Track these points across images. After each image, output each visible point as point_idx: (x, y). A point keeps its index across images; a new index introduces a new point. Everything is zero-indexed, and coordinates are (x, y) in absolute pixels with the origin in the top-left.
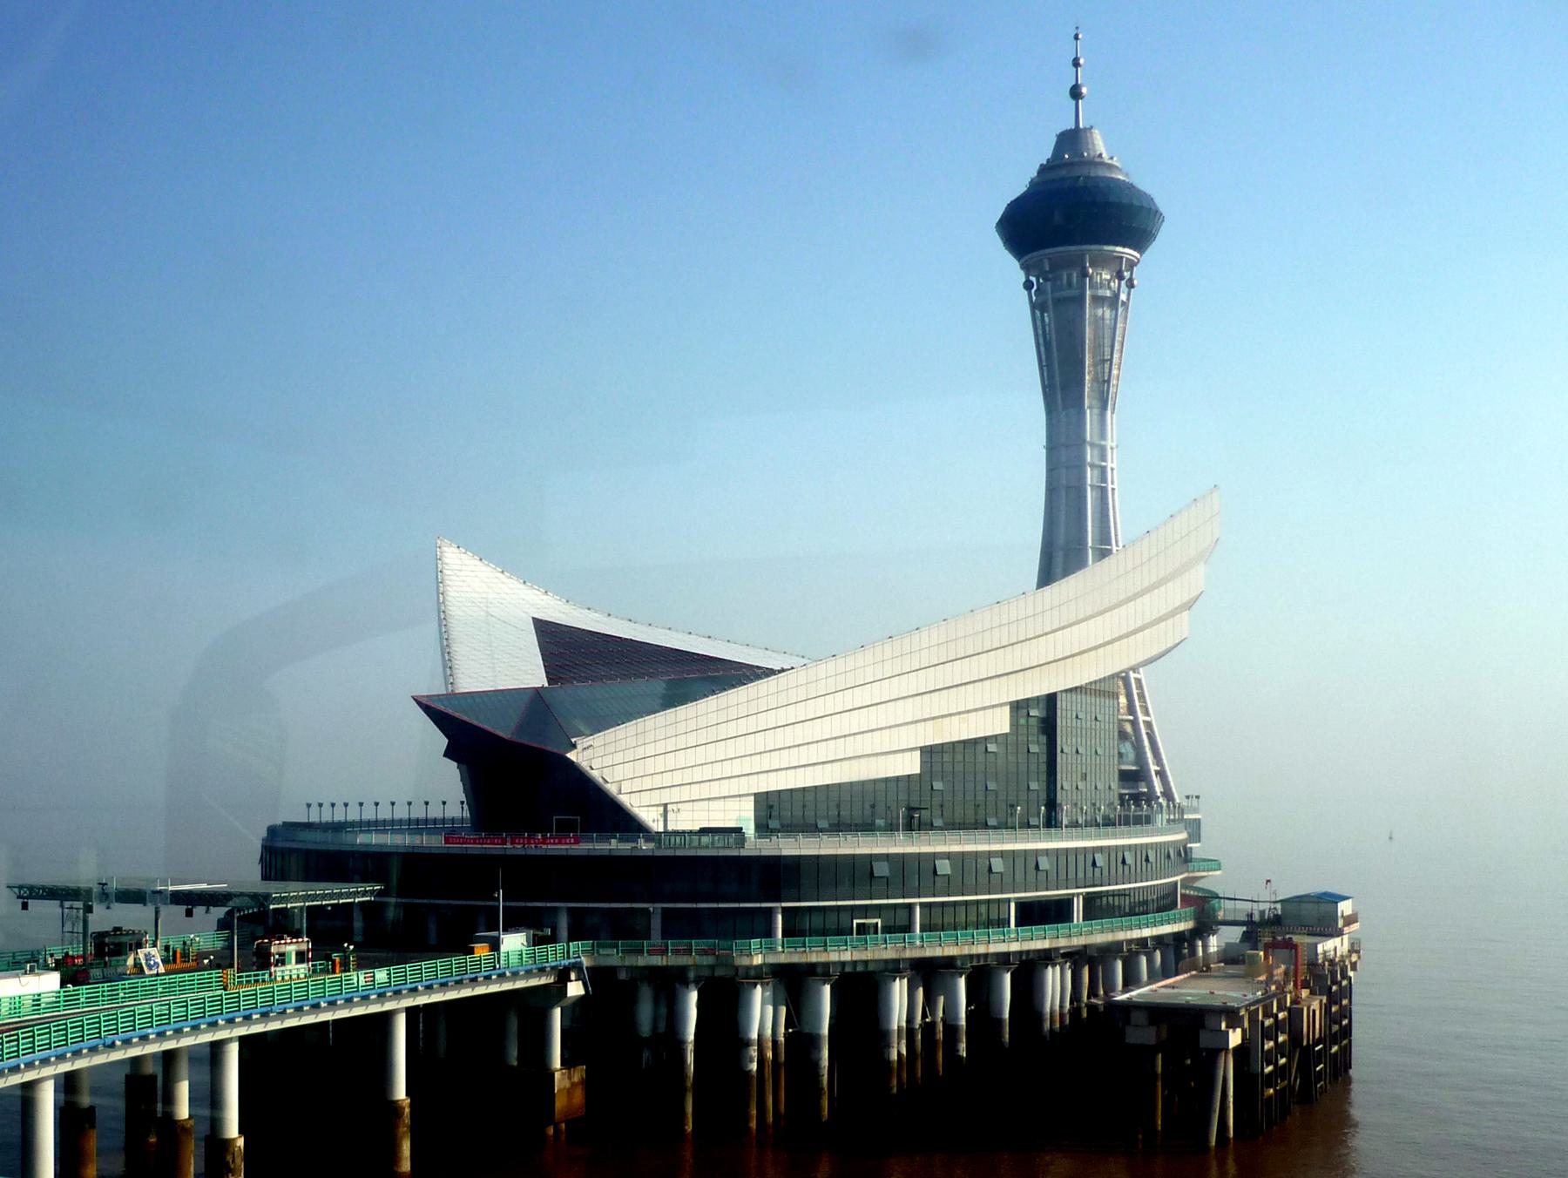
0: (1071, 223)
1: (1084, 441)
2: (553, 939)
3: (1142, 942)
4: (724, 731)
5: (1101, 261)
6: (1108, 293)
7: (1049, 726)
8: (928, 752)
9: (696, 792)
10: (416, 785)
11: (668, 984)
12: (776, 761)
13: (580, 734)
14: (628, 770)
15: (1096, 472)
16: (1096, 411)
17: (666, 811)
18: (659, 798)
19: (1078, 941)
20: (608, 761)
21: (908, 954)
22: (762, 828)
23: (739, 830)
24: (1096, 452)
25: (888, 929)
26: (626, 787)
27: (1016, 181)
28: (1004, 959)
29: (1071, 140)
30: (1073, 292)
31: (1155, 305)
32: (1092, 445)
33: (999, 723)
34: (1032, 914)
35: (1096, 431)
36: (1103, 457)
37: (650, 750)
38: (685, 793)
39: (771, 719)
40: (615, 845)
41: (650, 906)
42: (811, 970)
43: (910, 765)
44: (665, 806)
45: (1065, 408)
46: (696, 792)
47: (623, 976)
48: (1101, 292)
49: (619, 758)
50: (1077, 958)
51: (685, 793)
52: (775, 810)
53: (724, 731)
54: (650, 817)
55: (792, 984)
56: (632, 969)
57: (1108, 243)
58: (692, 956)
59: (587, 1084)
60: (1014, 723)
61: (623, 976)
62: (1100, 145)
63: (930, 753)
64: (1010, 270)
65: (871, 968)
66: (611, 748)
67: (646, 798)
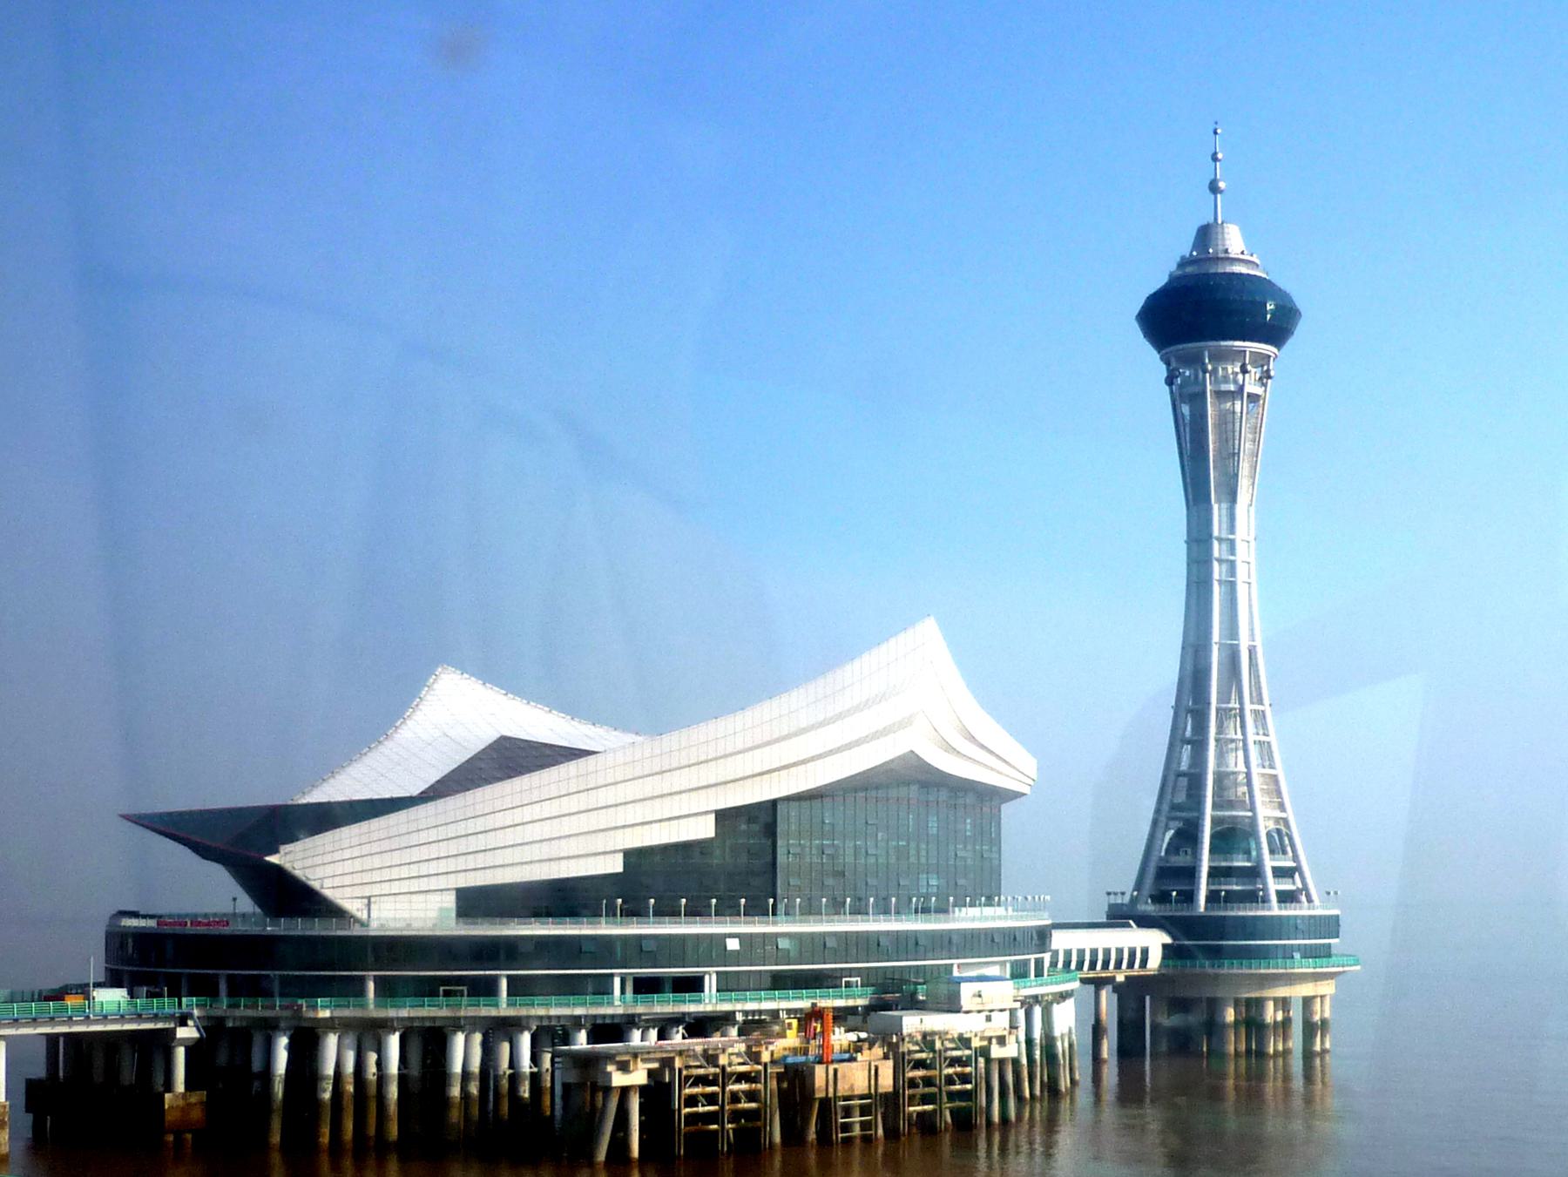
0: (1202, 313)
1: (1211, 536)
2: (160, 995)
4: (414, 839)
5: (1220, 357)
6: (1232, 387)
7: (771, 831)
8: (628, 854)
9: (396, 887)
11: (269, 1028)
14: (329, 870)
15: (1224, 567)
16: (1224, 506)
17: (369, 905)
18: (358, 891)
20: (309, 862)
24: (1224, 546)
26: (328, 883)
27: (1157, 279)
29: (1206, 234)
30: (1197, 389)
31: (1276, 394)
32: (1220, 540)
33: (705, 829)
35: (1224, 526)
36: (1232, 551)
37: (347, 854)
38: (386, 888)
39: (461, 828)
40: (299, 927)
43: (615, 865)
44: (369, 898)
46: (396, 887)
48: (1224, 387)
49: (318, 860)
51: (386, 888)
52: (472, 902)
53: (414, 839)
54: (353, 906)
57: (1224, 339)
59: (208, 1106)
62: (1234, 240)
64: (1149, 363)
65: (438, 1024)
66: (308, 853)
67: (348, 892)
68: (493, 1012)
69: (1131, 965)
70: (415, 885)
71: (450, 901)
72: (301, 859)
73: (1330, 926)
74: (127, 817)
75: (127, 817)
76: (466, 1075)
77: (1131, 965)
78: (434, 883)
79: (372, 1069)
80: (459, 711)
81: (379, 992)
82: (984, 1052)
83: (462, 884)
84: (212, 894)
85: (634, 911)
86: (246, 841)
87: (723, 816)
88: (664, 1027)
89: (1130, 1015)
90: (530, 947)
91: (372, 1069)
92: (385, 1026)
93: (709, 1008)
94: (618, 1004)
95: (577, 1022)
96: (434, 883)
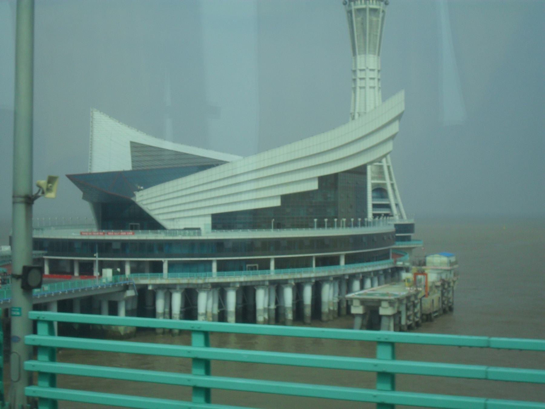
3: (369, 273)
9: (186, 214)
10: (71, 219)
12: (220, 201)
13: (139, 190)
19: (340, 273)
21: (268, 278)
22: (215, 226)
23: (199, 229)
25: (260, 269)
28: (308, 280)
33: (314, 186)
34: (323, 262)
41: (162, 259)
42: (228, 285)
45: (359, 54)
47: (150, 288)
50: (339, 279)
52: (221, 221)
55: (221, 290)
56: (154, 285)
58: (185, 279)
60: (282, 202)
61: (150, 288)
63: (285, 198)
75: (228, 162)
96: (202, 212)
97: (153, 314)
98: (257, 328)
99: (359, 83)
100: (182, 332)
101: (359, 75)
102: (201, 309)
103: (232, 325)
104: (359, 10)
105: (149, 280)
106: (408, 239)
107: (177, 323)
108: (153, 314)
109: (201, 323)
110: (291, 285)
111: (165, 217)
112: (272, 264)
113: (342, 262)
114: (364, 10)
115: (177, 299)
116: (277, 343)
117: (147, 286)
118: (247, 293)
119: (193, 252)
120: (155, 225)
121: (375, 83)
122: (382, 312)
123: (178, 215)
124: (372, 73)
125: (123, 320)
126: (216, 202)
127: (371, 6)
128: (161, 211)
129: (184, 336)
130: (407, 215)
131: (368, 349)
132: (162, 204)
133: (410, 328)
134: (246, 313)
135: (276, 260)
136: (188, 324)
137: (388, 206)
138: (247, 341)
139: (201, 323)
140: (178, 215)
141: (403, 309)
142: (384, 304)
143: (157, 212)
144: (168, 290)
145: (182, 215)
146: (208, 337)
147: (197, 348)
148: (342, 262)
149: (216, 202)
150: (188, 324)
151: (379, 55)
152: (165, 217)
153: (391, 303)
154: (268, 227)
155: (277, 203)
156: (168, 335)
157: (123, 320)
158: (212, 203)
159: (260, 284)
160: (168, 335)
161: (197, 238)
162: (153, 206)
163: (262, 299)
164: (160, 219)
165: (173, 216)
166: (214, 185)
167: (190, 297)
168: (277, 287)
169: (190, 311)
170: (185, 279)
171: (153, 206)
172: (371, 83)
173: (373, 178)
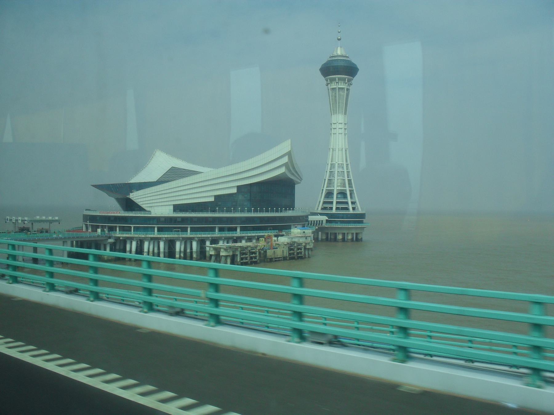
9: (158, 204)
13: (132, 192)
22: (175, 210)
33: (235, 191)
46: (158, 204)
52: (177, 208)
68: (236, 235)
69: (319, 225)
70: (161, 204)
71: (172, 208)
72: (135, 196)
73: (362, 216)
74: (93, 186)
75: (93, 186)
76: (180, 252)
77: (319, 225)
78: (167, 203)
79: (188, 250)
80: (159, 164)
81: (158, 231)
82: (305, 247)
83: (216, 194)
84: (111, 207)
85: (214, 211)
86: (123, 193)
87: (239, 187)
88: (228, 239)
89: (316, 237)
90: (180, 220)
91: (188, 250)
92: (191, 239)
93: (216, 236)
94: (217, 234)
95: (207, 238)
96: (167, 203)
97: (124, 251)
98: (177, 261)
99: (333, 131)
100: (136, 260)
101: (333, 126)
102: (146, 249)
103: (162, 258)
104: (333, 89)
105: (125, 235)
106: (361, 222)
107: (134, 256)
108: (124, 251)
109: (145, 256)
110: (163, 240)
111: (147, 205)
112: (189, 229)
113: (238, 230)
114: (336, 88)
115: (134, 244)
116: (187, 269)
117: (120, 237)
118: (171, 243)
119: (165, 223)
120: (141, 209)
121: (342, 131)
122: (222, 254)
123: (153, 205)
124: (340, 125)
125: (107, 253)
126: (174, 198)
127: (339, 87)
128: (144, 203)
129: (138, 262)
130: (361, 208)
131: (202, 271)
132: (144, 199)
133: (246, 264)
134: (171, 253)
135: (134, 227)
136: (139, 257)
137: (347, 203)
138: (170, 267)
139: (145, 256)
140: (153, 205)
141: (238, 253)
142: (222, 250)
143: (142, 203)
144: (131, 239)
145: (156, 204)
146: (150, 264)
147: (144, 269)
148: (238, 230)
149: (177, 198)
150: (139, 257)
151: (345, 113)
152: (147, 205)
153: (226, 250)
154: (207, 211)
155: (212, 199)
156: (130, 261)
157: (107, 253)
158: (172, 199)
159: (178, 239)
160: (130, 261)
161: (149, 215)
162: (139, 200)
163: (179, 246)
164: (144, 206)
165: (151, 205)
166: (173, 190)
167: (140, 243)
168: (187, 241)
169: (140, 251)
170: (142, 235)
171: (139, 200)
172: (340, 131)
173: (338, 186)
